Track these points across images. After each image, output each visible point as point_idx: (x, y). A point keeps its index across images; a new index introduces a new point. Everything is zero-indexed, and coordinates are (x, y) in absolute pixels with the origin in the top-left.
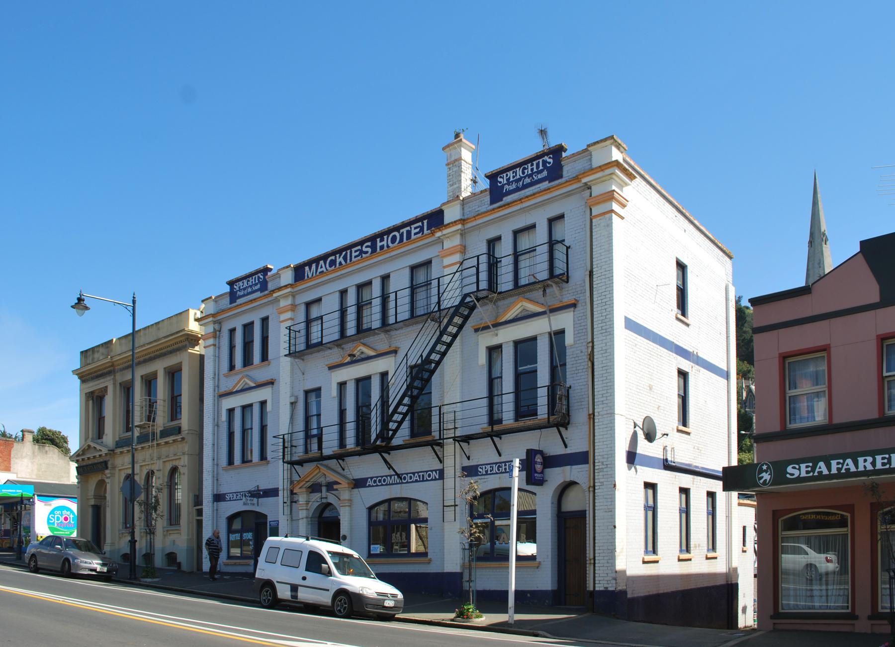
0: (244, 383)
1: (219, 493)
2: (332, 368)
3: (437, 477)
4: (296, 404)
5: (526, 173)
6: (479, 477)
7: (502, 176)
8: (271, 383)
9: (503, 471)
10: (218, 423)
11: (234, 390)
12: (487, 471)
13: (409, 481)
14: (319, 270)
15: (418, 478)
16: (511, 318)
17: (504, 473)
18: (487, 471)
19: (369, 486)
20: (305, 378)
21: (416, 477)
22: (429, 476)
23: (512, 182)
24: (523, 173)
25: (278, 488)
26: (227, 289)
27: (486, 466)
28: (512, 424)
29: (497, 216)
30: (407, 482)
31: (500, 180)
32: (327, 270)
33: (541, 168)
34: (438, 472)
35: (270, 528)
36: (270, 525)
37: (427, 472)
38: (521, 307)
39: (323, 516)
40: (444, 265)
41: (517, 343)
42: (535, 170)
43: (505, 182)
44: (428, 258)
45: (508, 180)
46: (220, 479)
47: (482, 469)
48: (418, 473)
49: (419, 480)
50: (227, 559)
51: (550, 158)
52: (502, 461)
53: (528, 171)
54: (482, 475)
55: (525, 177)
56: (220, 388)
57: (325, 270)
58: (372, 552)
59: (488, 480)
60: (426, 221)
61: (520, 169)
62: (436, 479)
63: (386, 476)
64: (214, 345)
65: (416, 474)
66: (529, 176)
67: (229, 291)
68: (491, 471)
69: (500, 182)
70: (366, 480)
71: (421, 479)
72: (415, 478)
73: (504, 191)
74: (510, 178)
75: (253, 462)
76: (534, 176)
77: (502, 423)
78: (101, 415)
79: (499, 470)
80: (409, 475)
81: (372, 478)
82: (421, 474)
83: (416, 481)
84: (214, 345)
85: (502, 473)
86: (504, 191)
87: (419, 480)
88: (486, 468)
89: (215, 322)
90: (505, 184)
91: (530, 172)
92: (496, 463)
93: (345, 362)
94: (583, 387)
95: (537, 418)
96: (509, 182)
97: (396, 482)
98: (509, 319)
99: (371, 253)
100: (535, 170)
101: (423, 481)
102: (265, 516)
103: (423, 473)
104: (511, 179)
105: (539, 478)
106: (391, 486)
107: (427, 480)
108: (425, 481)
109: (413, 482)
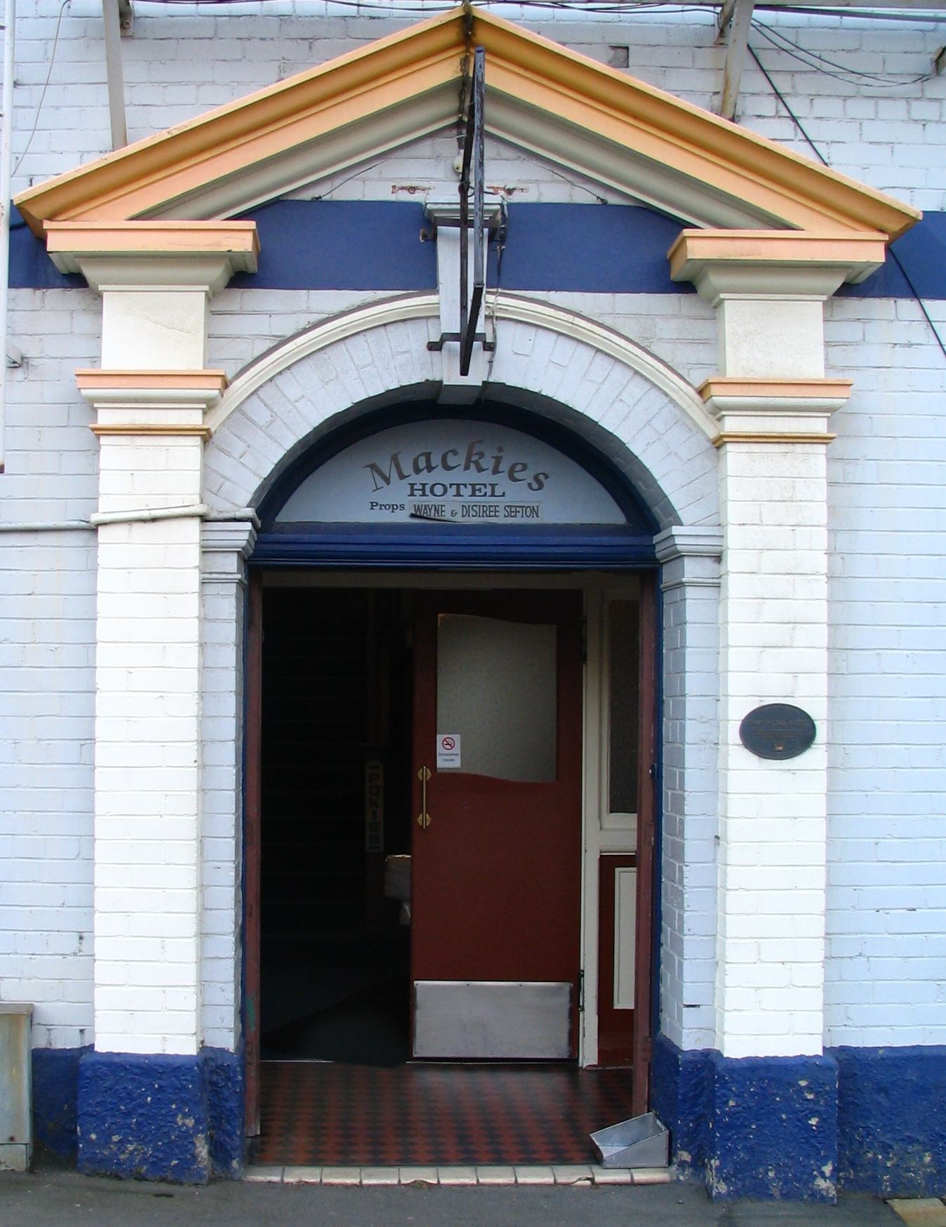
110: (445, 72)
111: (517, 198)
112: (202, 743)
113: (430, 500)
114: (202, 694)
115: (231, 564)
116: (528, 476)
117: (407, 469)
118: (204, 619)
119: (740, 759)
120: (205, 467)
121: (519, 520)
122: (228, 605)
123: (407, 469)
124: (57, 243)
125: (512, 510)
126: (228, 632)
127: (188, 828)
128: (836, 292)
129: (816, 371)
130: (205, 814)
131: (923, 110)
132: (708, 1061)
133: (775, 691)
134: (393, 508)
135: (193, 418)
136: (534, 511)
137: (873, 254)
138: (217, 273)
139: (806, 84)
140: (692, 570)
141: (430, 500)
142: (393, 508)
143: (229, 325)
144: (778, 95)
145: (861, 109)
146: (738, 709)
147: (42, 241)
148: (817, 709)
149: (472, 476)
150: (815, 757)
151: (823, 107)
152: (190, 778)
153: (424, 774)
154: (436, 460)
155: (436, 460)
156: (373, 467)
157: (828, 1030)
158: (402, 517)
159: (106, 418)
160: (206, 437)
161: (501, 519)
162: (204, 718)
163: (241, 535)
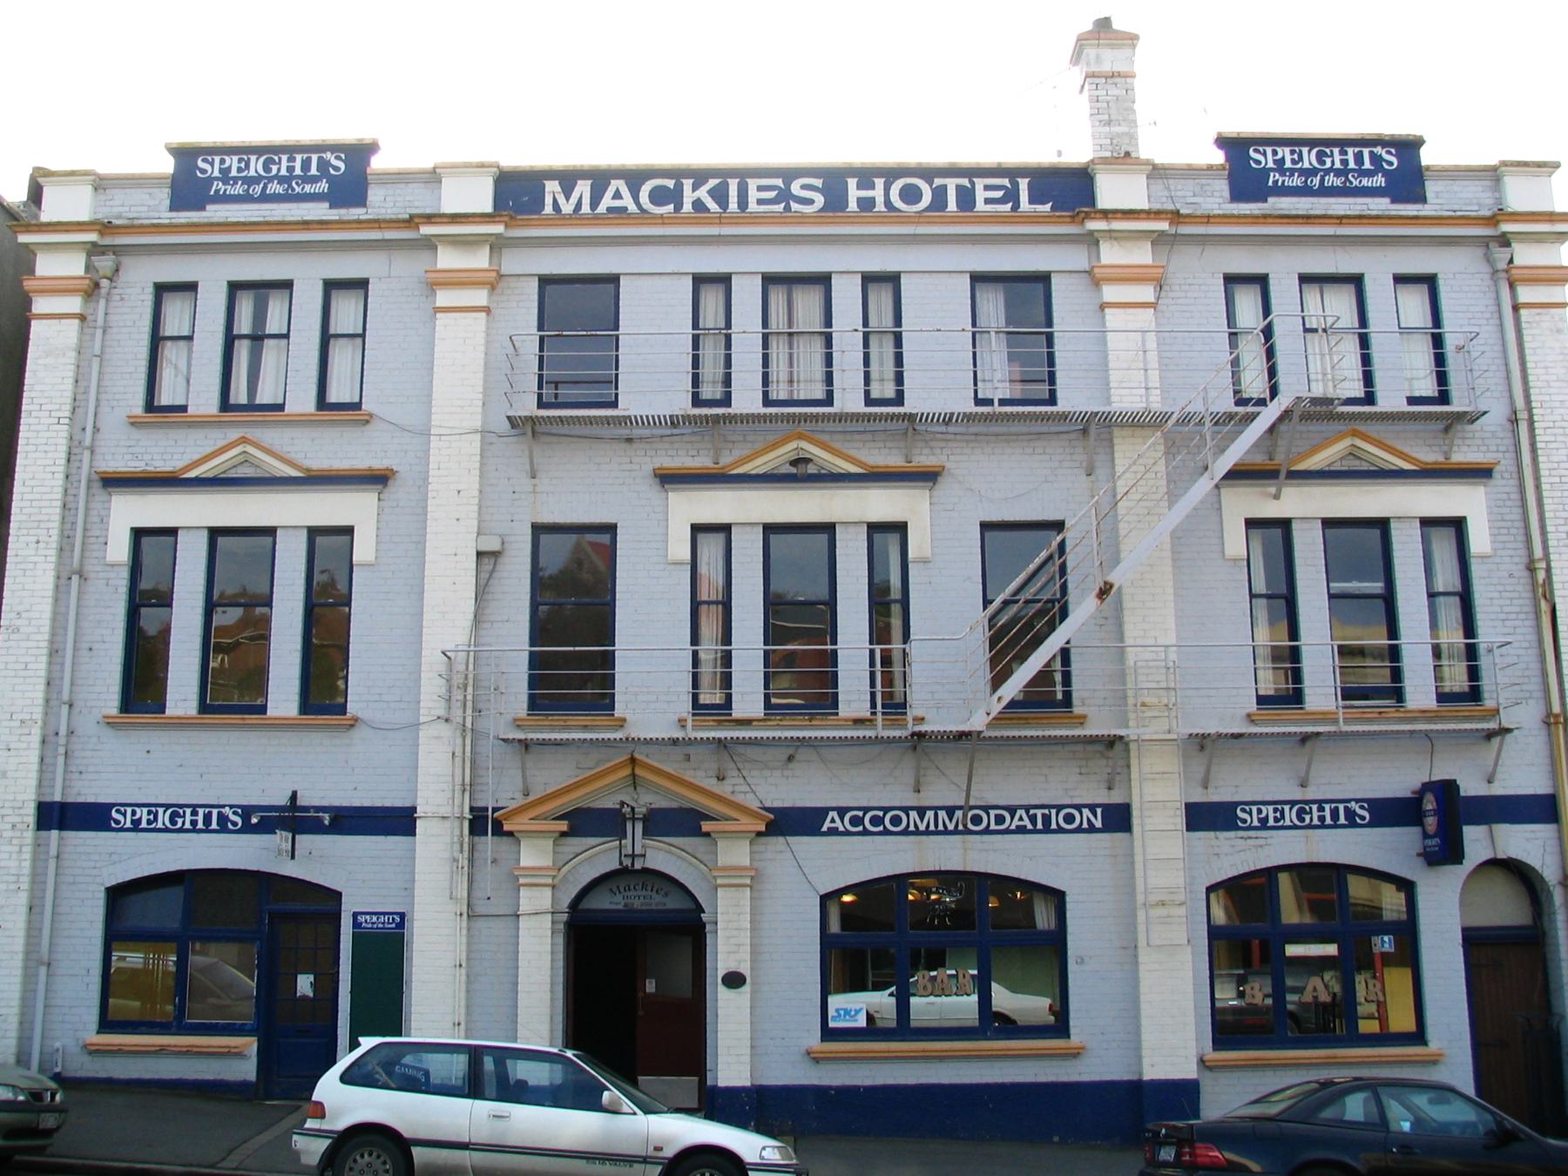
0: (241, 459)
1: (71, 799)
2: (669, 479)
3: (1098, 824)
4: (501, 560)
5: (274, 172)
6: (1241, 833)
7: (210, 158)
8: (379, 479)
9: (1316, 822)
10: (81, 564)
11: (192, 474)
12: (1264, 821)
13: (993, 826)
14: (607, 201)
15: (1027, 822)
16: (761, 471)
17: (187, 831)
18: (1264, 821)
19: (833, 832)
20: (538, 489)
21: (1021, 819)
22: (1069, 819)
23: (235, 179)
24: (267, 168)
25: (414, 809)
26: (167, 165)
27: (136, 809)
28: (294, 719)
29: (184, 242)
30: (987, 831)
31: (200, 164)
32: (888, 203)
33: (314, 171)
34: (1099, 811)
35: (356, 938)
36: (356, 924)
37: (1059, 808)
38: (240, 454)
39: (581, 907)
40: (438, 305)
41: (314, 532)
42: (298, 171)
43: (216, 174)
44: (614, 272)
45: (225, 172)
46: (77, 754)
47: (124, 815)
48: (1027, 808)
49: (1030, 827)
50: (98, 1033)
51: (338, 158)
52: (1310, 796)
53: (279, 170)
54: (1250, 828)
55: (271, 179)
56: (98, 457)
57: (880, 200)
58: (832, 1024)
59: (1269, 841)
60: (1027, 180)
61: (257, 159)
62: (1092, 829)
63: (906, 810)
64: (82, 318)
65: (1020, 812)
66: (282, 180)
67: (171, 171)
68: (149, 822)
69: (204, 171)
70: (822, 812)
71: (1040, 826)
72: (1016, 822)
73: (212, 193)
74: (229, 168)
75: (270, 713)
76: (294, 184)
77: (164, 712)
78: (1122, 426)
79: (173, 822)
80: (993, 813)
81: (842, 811)
82: (1039, 813)
83: (1021, 830)
84: (82, 318)
85: (1310, 827)
86: (212, 193)
87: (1030, 827)
88: (134, 813)
89: (94, 250)
90: (217, 179)
91: (284, 172)
92: (1292, 803)
93: (732, 472)
94: (1522, 652)
95: (613, 715)
96: (225, 176)
97: (941, 827)
98: (754, 472)
99: (821, 210)
100: (298, 171)
101: (1047, 829)
102: (336, 896)
103: (1046, 811)
104: (234, 173)
105: (1433, 849)
106: (924, 838)
107: (1060, 830)
108: (1054, 832)
109: (1007, 831)
110: (627, 771)
111: (653, 806)
112: (552, 985)
113: (629, 901)
114: (552, 953)
115: (562, 926)
116: (663, 892)
117: (622, 890)
118: (552, 945)
119: (721, 988)
120: (553, 895)
121: (660, 907)
122: (560, 940)
123: (622, 890)
124: (506, 828)
125: (657, 904)
126: (560, 948)
127: (547, 1011)
128: (1227, 474)
129: (747, 862)
130: (552, 1006)
131: (786, 773)
132: (715, 1087)
133: (733, 967)
134: (617, 904)
135: (550, 881)
136: (665, 904)
137: (763, 828)
138: (557, 835)
139: (748, 765)
140: (708, 928)
141: (629, 901)
142: (617, 904)
143: (560, 849)
144: (739, 770)
145: (767, 773)
146: (721, 974)
147: (502, 825)
148: (747, 973)
149: (644, 893)
150: (747, 988)
151: (755, 773)
152: (548, 996)
153: (641, 994)
154: (632, 887)
155: (632, 887)
156: (611, 890)
157: (39, 794)
158: (620, 907)
159: (522, 881)
160: (553, 887)
161: (654, 907)
162: (552, 977)
163: (565, 917)
